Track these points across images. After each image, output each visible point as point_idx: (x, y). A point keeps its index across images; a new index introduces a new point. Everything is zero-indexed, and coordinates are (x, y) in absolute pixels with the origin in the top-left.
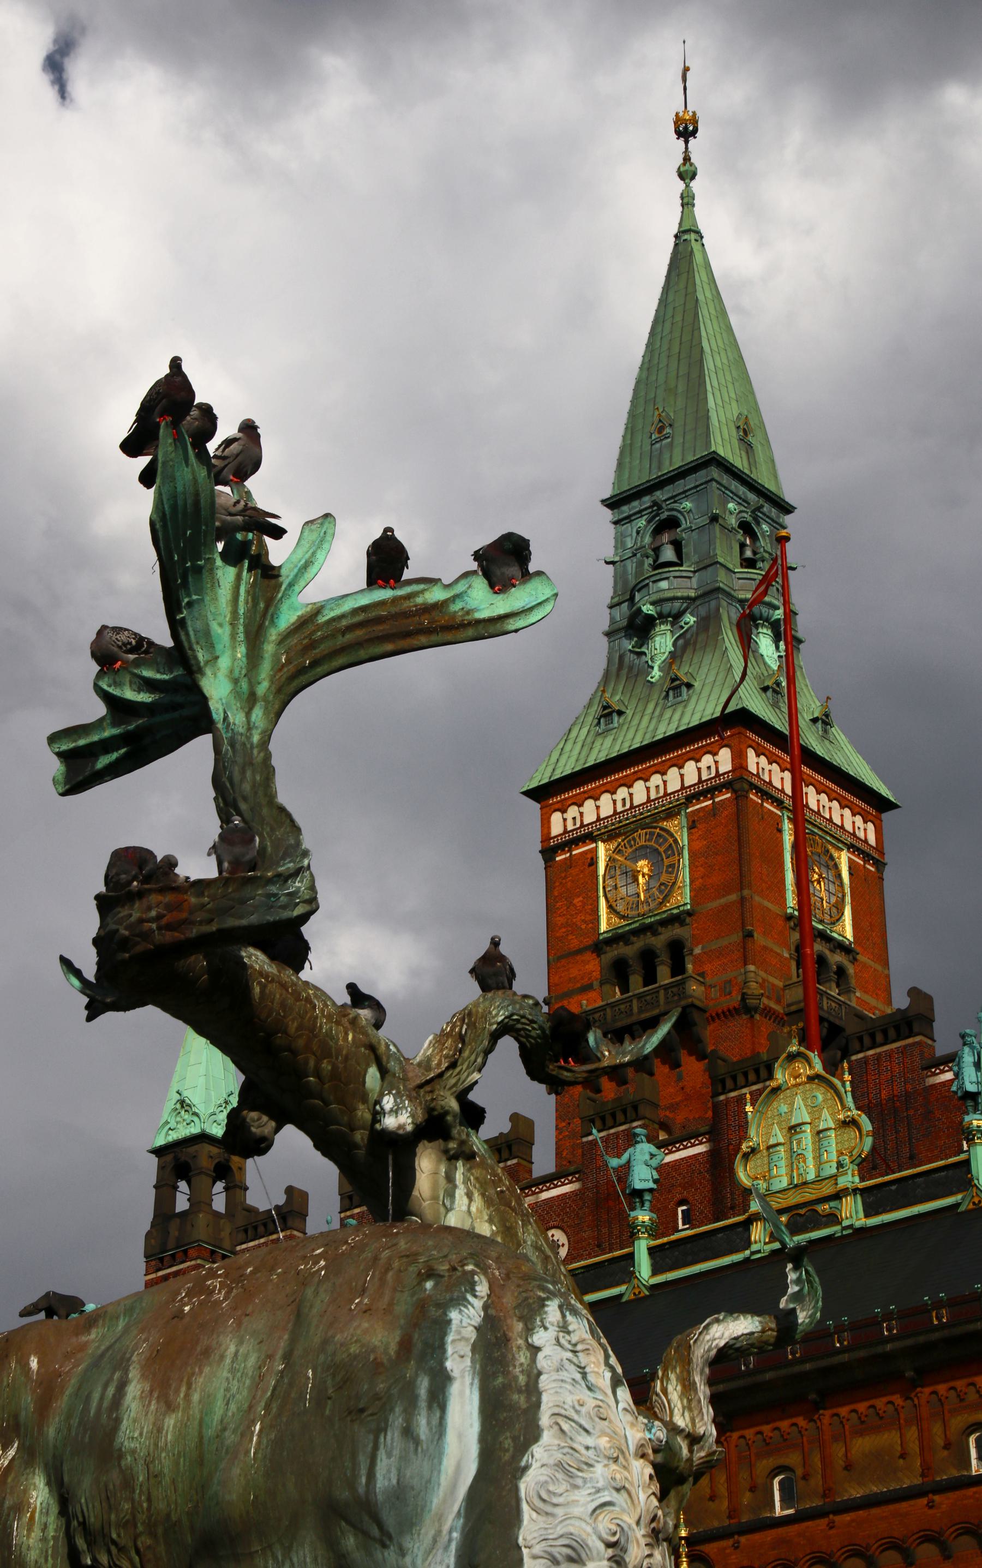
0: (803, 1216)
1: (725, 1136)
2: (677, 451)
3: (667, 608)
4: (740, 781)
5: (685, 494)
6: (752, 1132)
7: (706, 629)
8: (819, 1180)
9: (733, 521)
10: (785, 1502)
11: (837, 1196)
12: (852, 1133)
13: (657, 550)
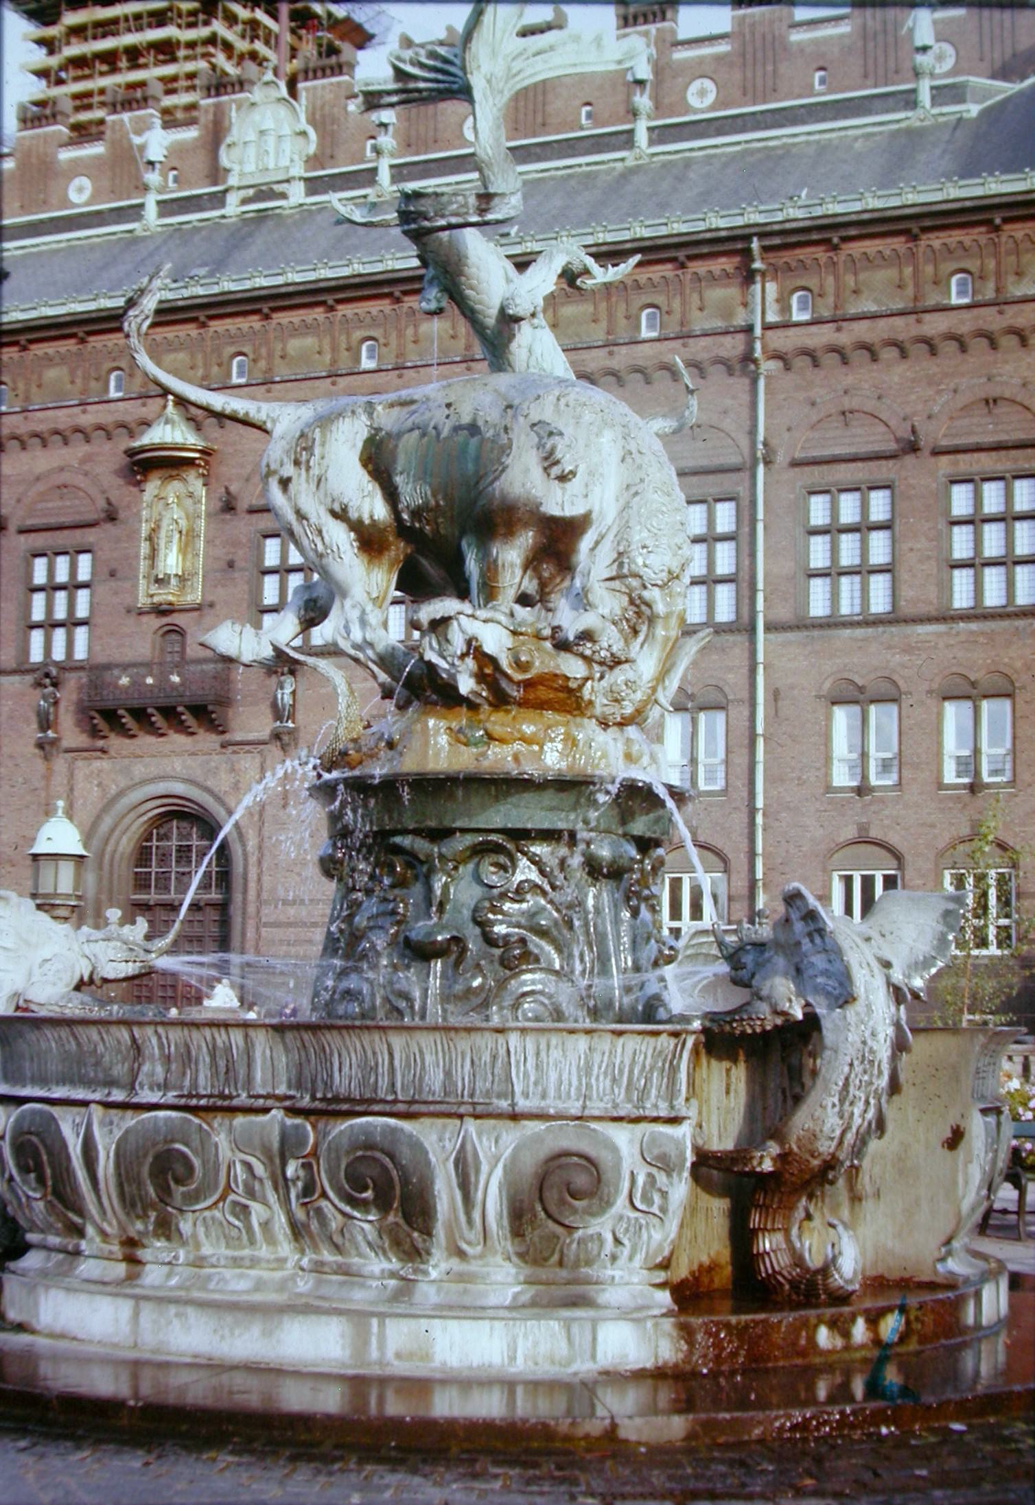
0: (264, 193)
1: (216, 134)
8: (277, 169)
10: (118, 388)
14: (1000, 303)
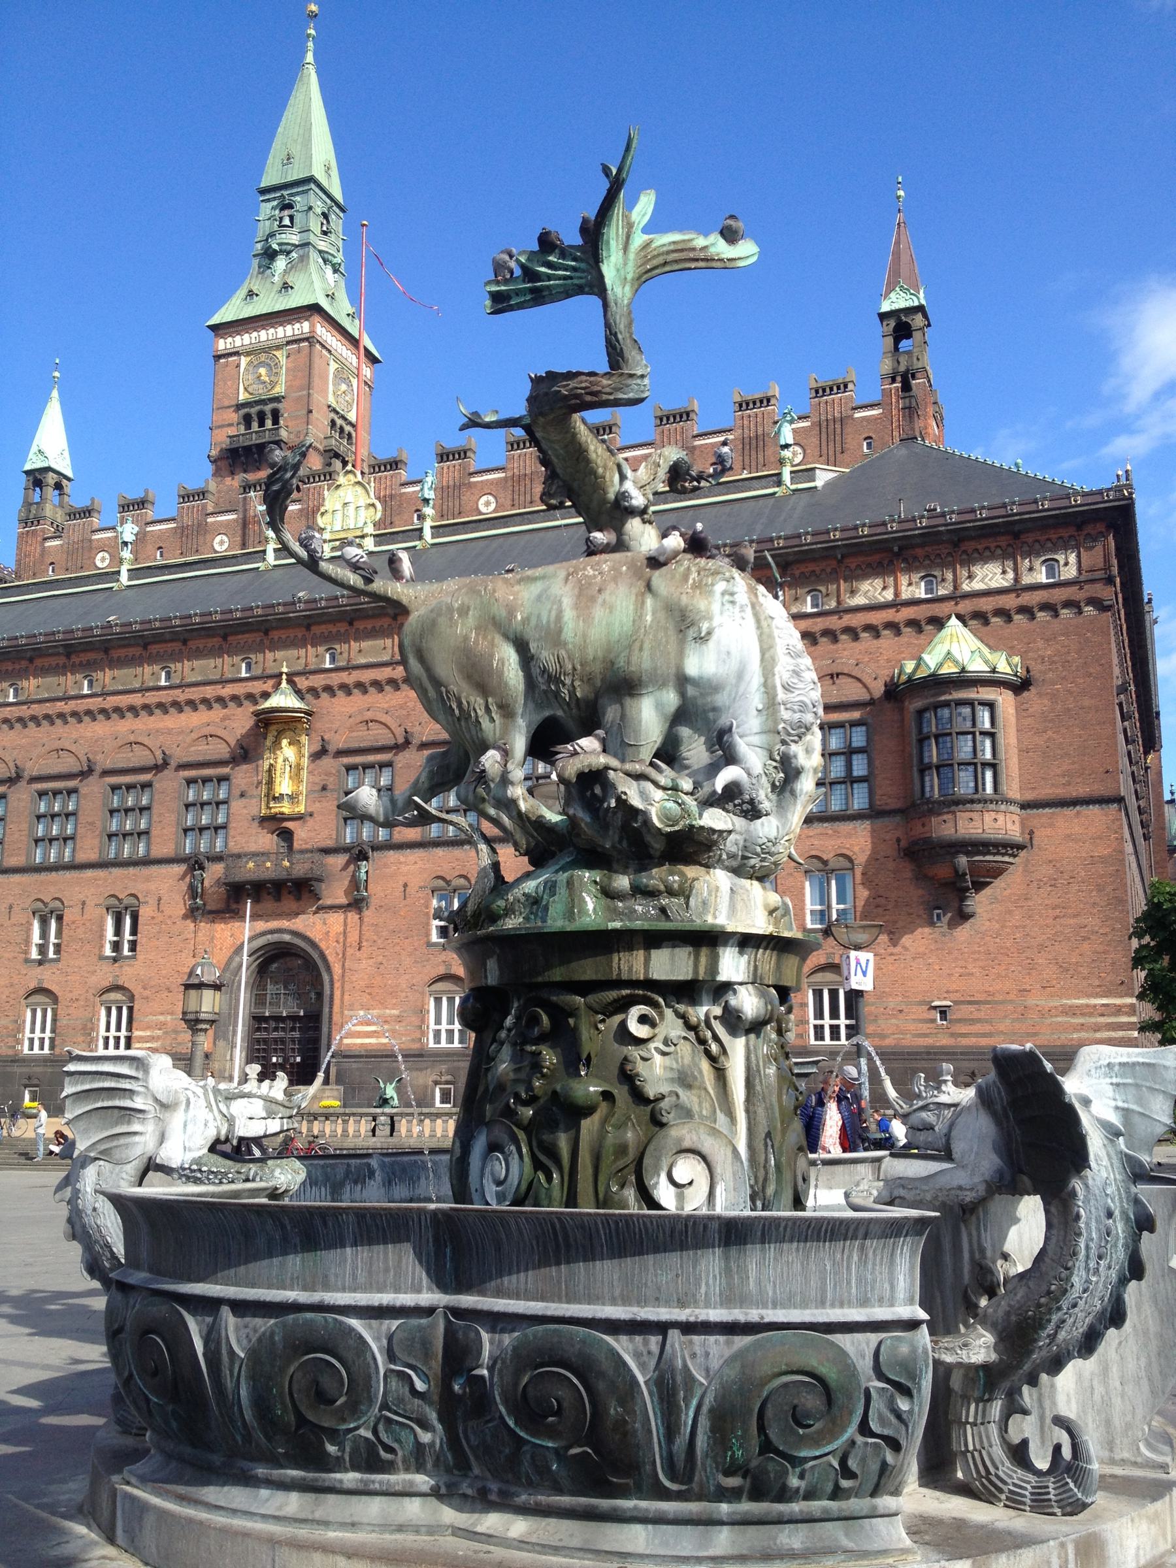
2: (295, 171)
3: (284, 247)
4: (310, 339)
5: (298, 194)
6: (326, 503)
7: (302, 261)
9: (319, 211)
11: (363, 537)
12: (372, 509)
13: (281, 219)
14: (840, 611)
